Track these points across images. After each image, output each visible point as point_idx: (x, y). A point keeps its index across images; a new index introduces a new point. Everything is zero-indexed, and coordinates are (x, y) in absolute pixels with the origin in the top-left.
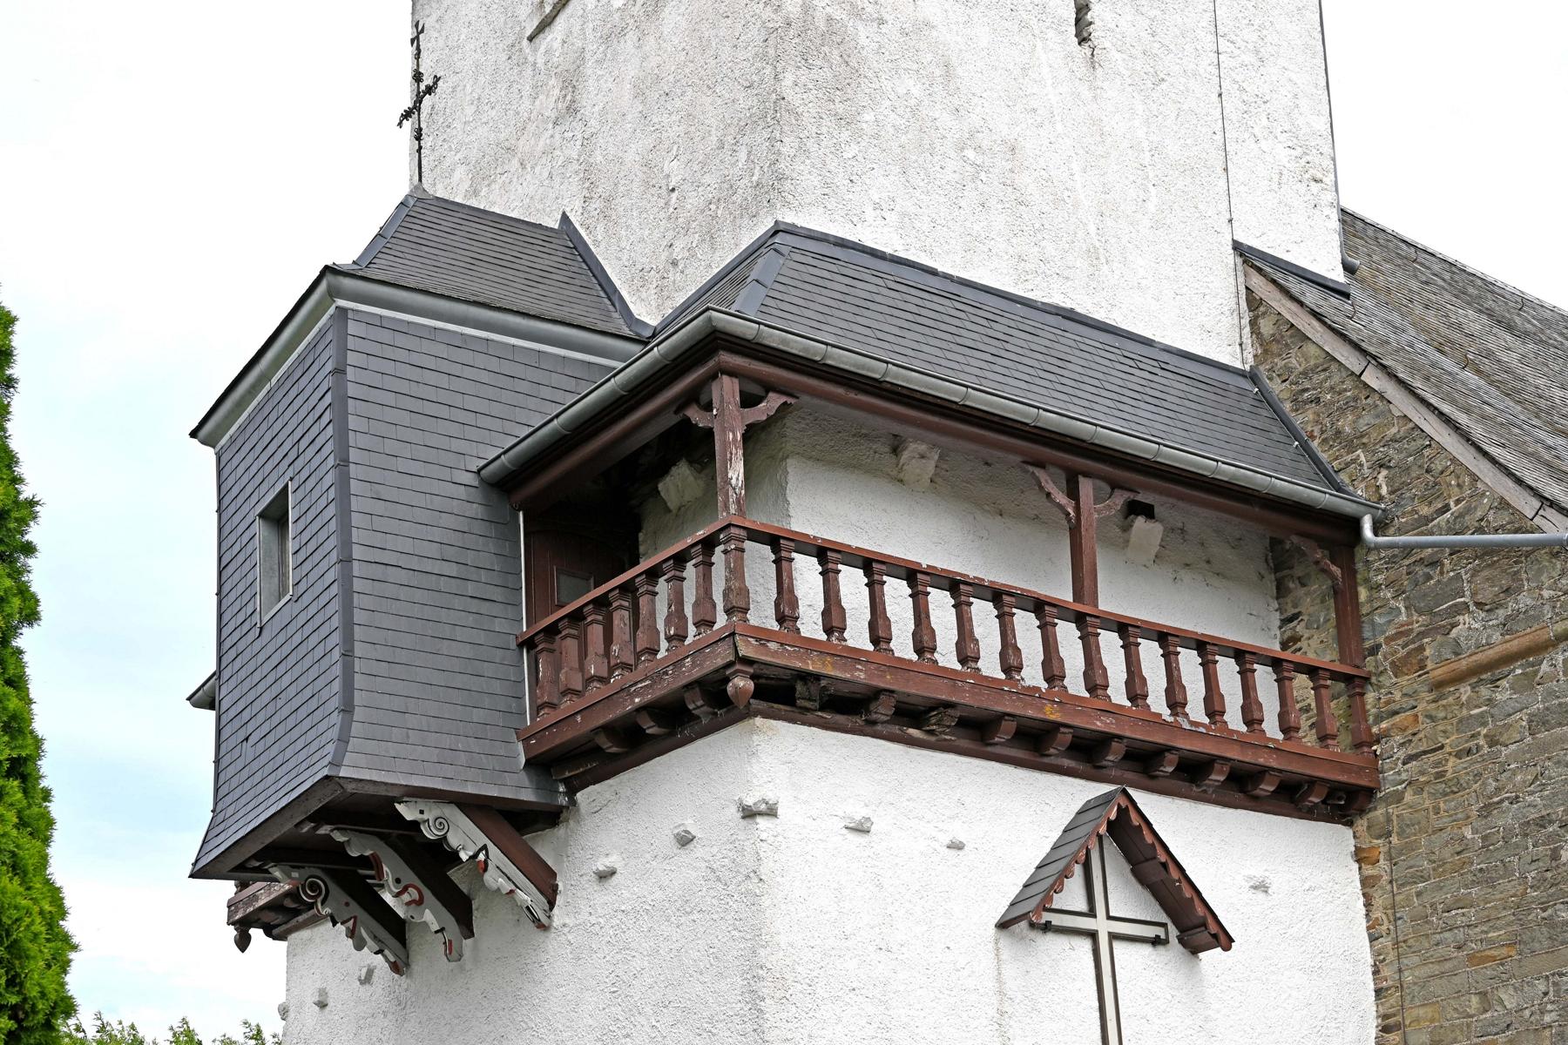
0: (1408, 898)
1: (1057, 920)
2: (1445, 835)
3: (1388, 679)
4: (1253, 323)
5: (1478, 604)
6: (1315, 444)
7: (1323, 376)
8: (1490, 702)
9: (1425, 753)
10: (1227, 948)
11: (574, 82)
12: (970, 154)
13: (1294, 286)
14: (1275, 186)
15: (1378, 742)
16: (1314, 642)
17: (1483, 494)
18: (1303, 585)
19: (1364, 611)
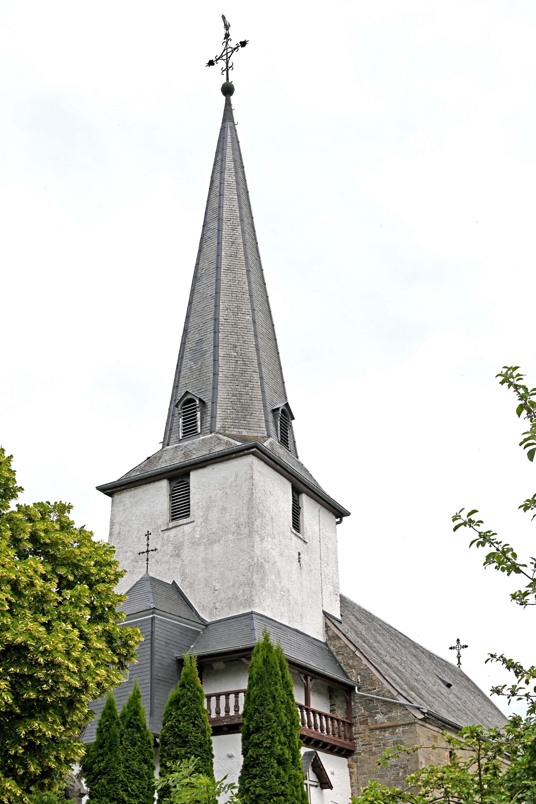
0: (361, 778)
2: (371, 765)
3: (358, 725)
4: (326, 631)
5: (381, 713)
6: (342, 665)
7: (345, 649)
8: (384, 736)
9: (367, 744)
10: (332, 789)
11: (179, 548)
12: (282, 592)
13: (333, 621)
15: (355, 740)
17: (384, 688)
18: (337, 698)
19: (353, 707)
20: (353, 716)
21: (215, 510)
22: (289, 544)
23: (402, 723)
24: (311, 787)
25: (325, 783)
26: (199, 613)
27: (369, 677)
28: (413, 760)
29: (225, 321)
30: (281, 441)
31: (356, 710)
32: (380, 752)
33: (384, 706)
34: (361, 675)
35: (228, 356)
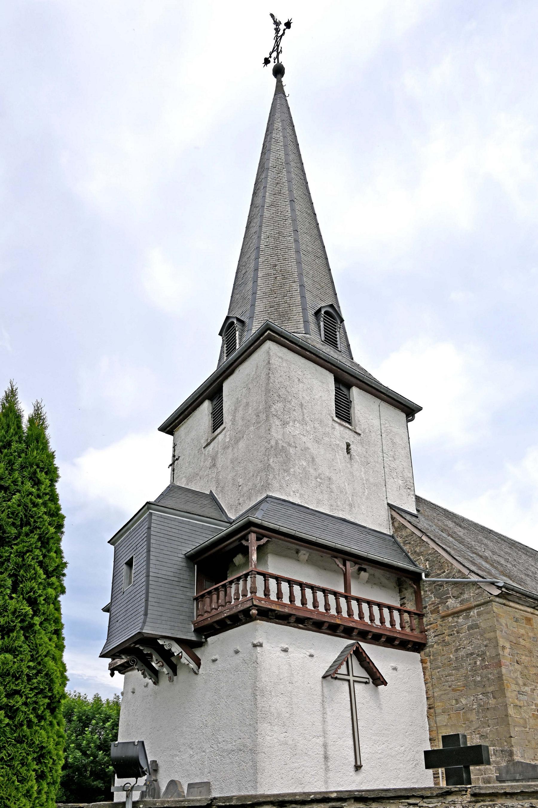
0: (435, 673)
1: (339, 676)
2: (445, 657)
3: (430, 615)
4: (393, 523)
6: (409, 554)
7: (411, 537)
8: (457, 622)
9: (440, 635)
14: (398, 490)
15: (427, 631)
16: (409, 605)
18: (406, 590)
19: (423, 597)
20: (424, 606)
21: (241, 408)
22: (330, 432)
23: (476, 603)
24: (355, 683)
25: (378, 679)
26: (228, 514)
27: (437, 561)
28: (492, 645)
29: (266, 247)
30: (325, 340)
31: (426, 600)
32: (454, 641)
33: (455, 589)
34: (429, 561)
35: (267, 275)
